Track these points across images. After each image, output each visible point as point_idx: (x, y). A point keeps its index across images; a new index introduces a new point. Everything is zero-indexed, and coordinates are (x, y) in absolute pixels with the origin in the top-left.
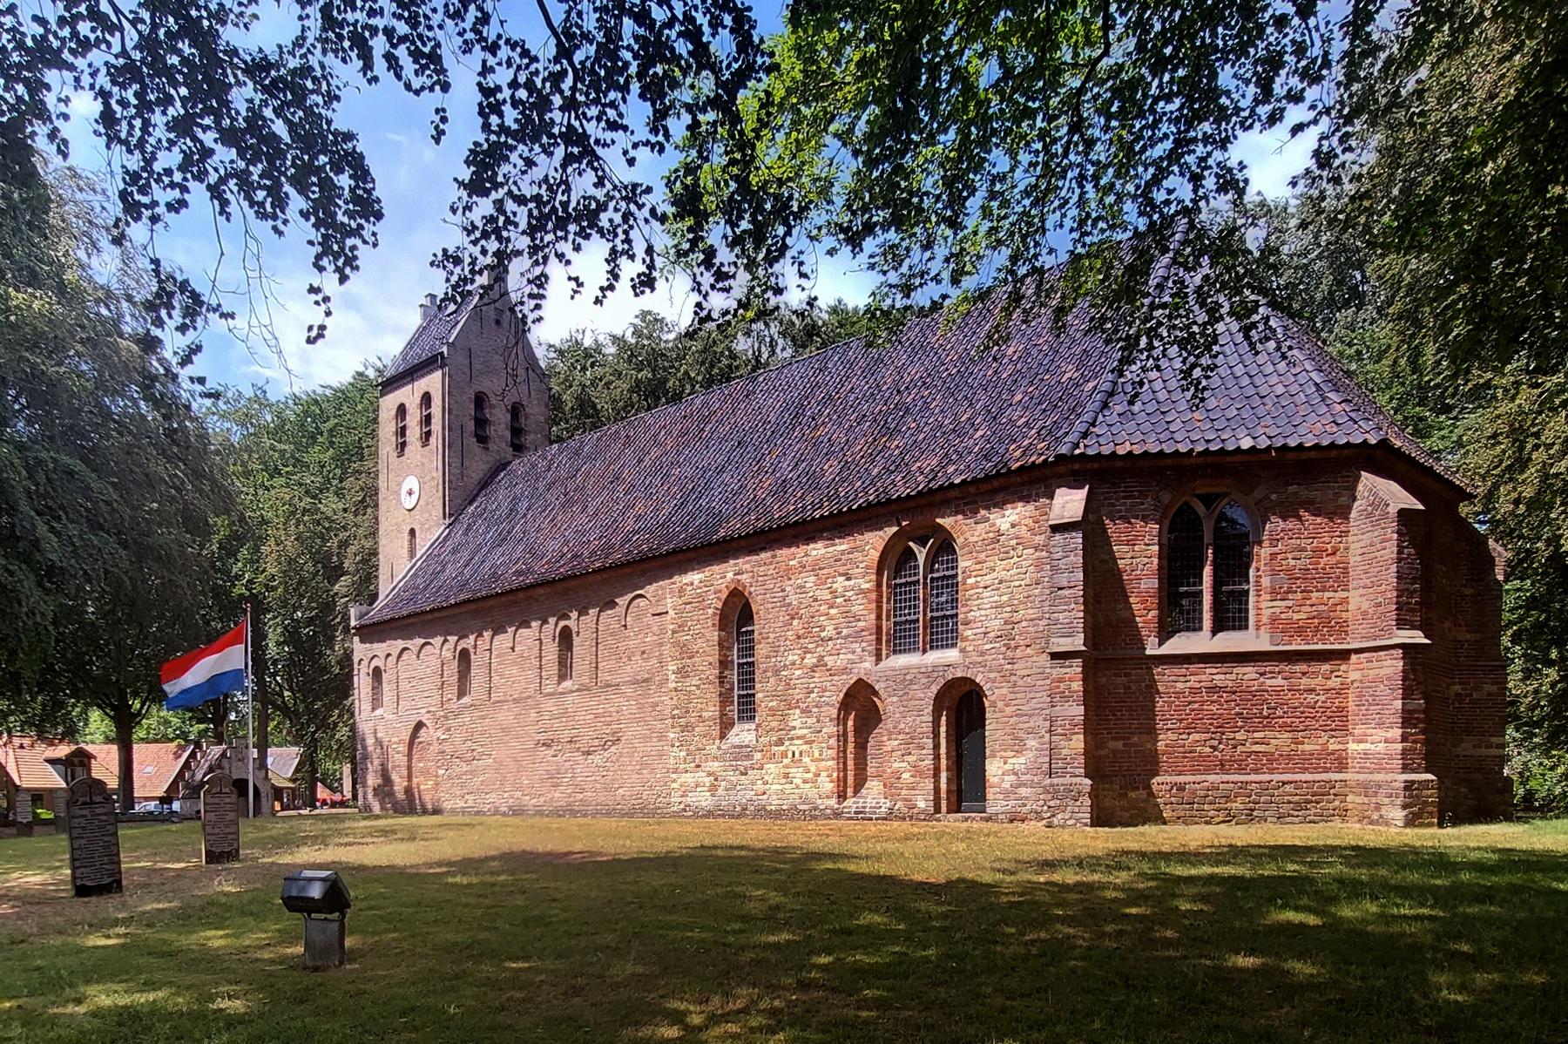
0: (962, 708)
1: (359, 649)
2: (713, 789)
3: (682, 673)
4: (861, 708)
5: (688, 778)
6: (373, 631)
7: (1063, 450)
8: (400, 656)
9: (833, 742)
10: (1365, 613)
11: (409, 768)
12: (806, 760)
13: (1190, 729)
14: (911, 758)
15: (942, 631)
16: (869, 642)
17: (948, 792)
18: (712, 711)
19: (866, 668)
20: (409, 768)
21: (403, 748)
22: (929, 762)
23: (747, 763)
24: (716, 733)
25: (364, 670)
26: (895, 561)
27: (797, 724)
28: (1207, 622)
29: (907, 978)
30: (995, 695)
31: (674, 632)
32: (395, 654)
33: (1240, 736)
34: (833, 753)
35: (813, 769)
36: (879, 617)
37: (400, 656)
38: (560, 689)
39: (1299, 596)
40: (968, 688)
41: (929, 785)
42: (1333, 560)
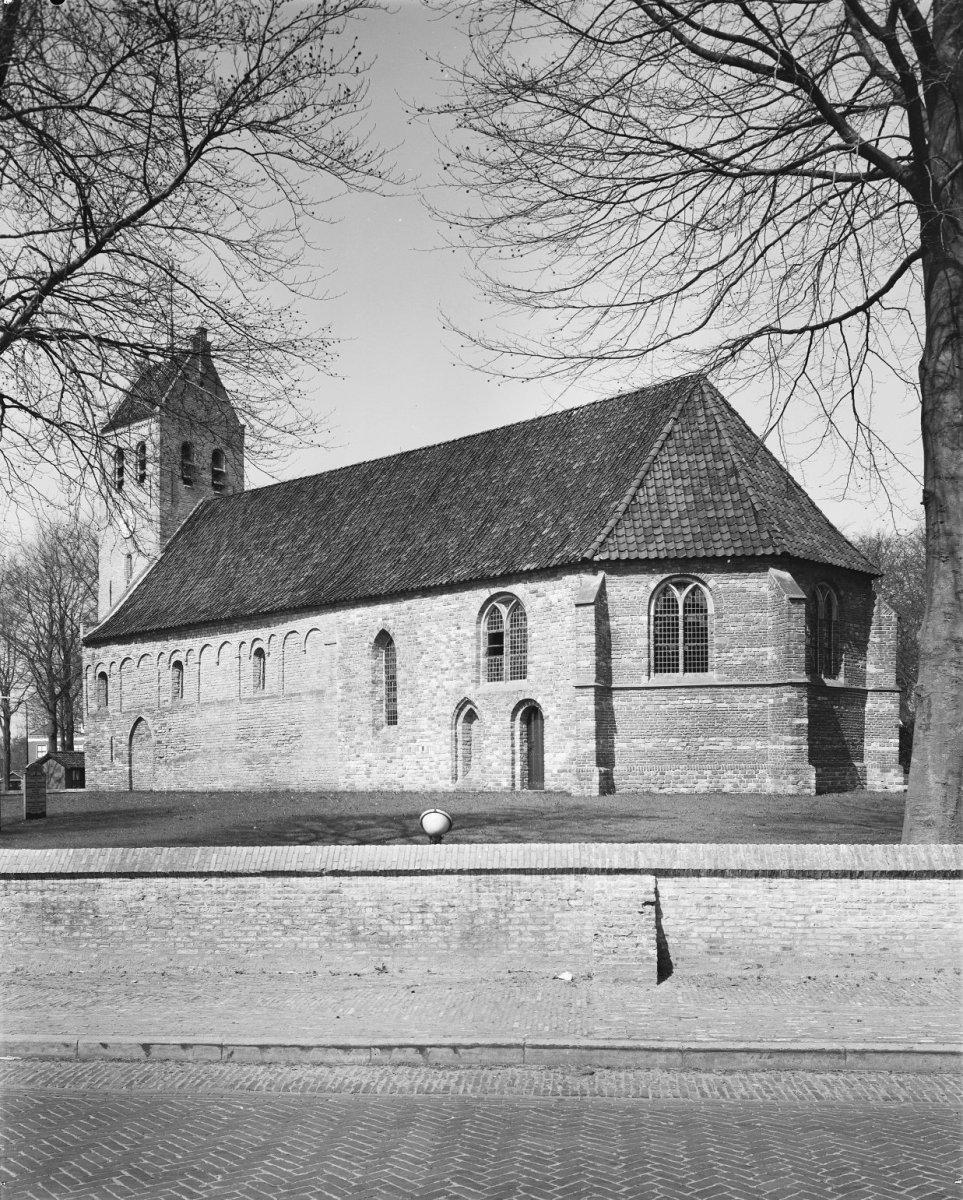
0: (530, 714)
1: (87, 653)
2: (368, 774)
3: (347, 688)
4: (467, 713)
5: (352, 765)
6: (94, 642)
7: (587, 555)
8: (123, 663)
9: (448, 740)
10: (774, 662)
11: (130, 755)
12: (432, 753)
13: (668, 735)
14: (497, 753)
15: (520, 672)
16: (469, 675)
17: (522, 774)
18: (367, 717)
19: (470, 692)
20: (130, 755)
21: (126, 739)
22: (509, 756)
23: (391, 755)
24: (370, 732)
25: (90, 676)
26: (489, 610)
27: (425, 727)
28: (681, 667)
29: (415, 741)
30: (548, 710)
31: (341, 658)
32: (118, 663)
33: (701, 739)
34: (448, 748)
35: (436, 759)
36: (478, 656)
37: (123, 663)
38: (256, 696)
39: (736, 650)
40: (904, 835)
41: (508, 768)
42: (757, 627)
